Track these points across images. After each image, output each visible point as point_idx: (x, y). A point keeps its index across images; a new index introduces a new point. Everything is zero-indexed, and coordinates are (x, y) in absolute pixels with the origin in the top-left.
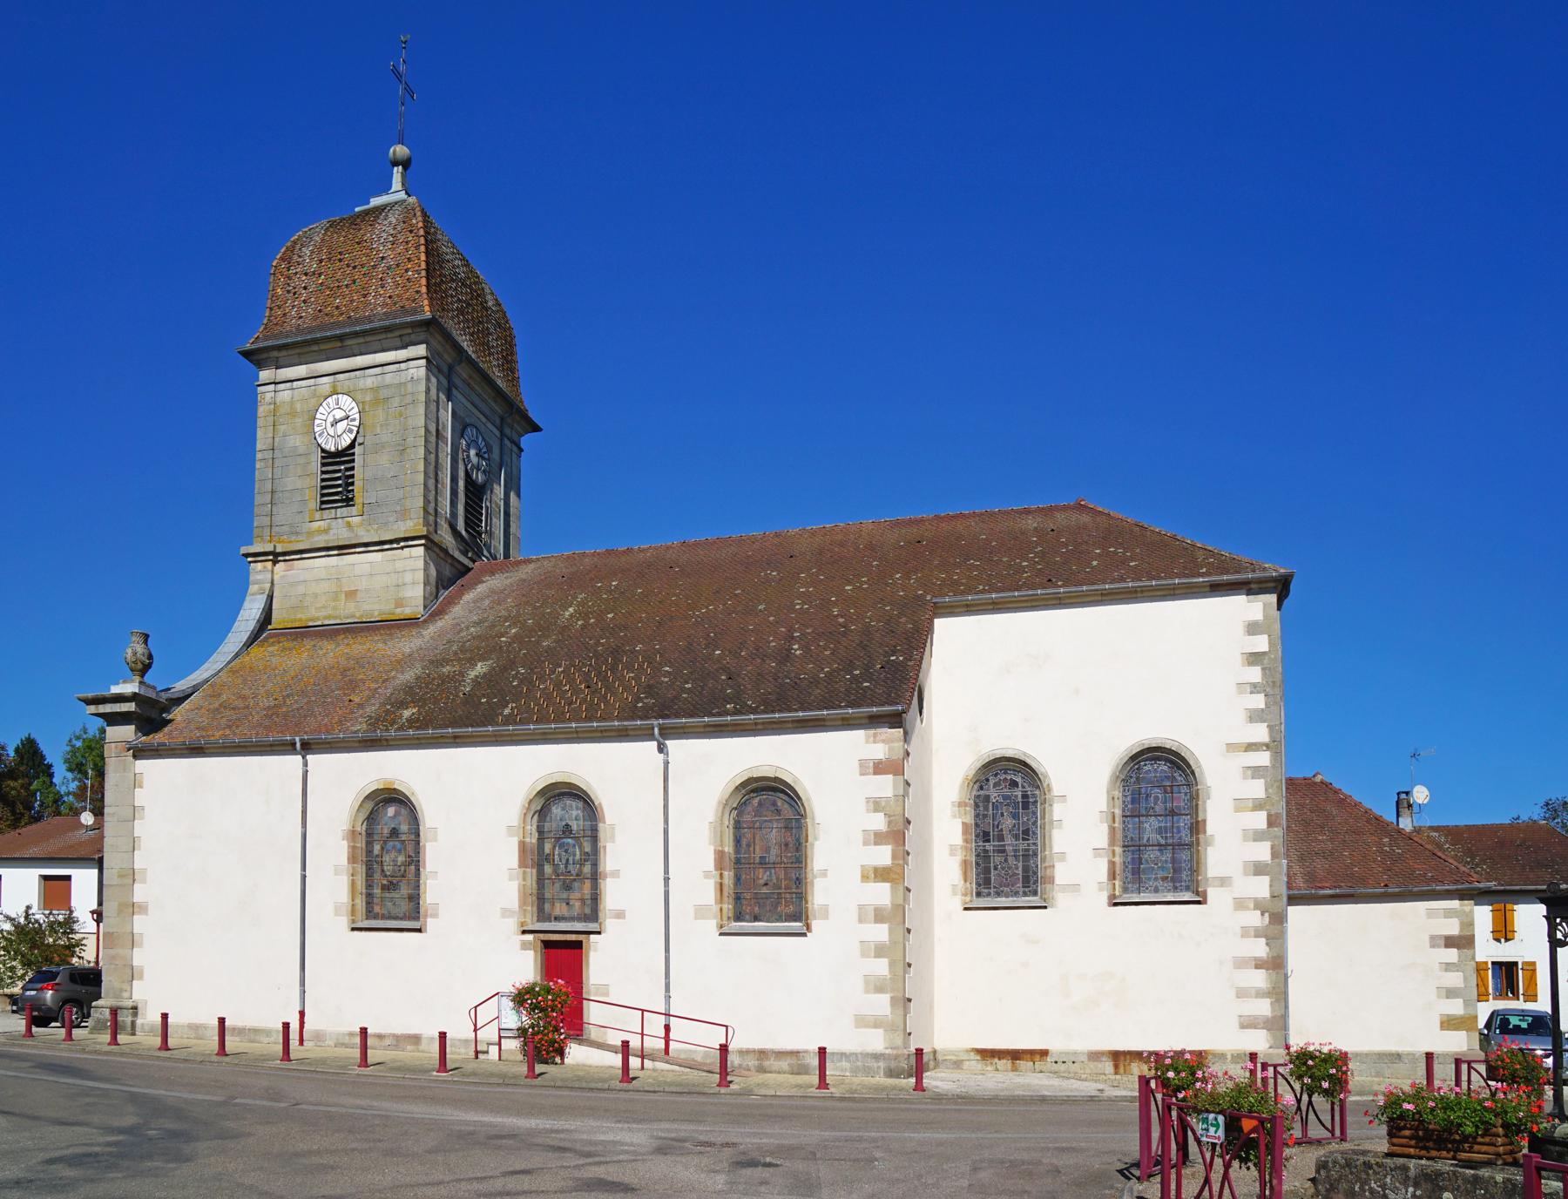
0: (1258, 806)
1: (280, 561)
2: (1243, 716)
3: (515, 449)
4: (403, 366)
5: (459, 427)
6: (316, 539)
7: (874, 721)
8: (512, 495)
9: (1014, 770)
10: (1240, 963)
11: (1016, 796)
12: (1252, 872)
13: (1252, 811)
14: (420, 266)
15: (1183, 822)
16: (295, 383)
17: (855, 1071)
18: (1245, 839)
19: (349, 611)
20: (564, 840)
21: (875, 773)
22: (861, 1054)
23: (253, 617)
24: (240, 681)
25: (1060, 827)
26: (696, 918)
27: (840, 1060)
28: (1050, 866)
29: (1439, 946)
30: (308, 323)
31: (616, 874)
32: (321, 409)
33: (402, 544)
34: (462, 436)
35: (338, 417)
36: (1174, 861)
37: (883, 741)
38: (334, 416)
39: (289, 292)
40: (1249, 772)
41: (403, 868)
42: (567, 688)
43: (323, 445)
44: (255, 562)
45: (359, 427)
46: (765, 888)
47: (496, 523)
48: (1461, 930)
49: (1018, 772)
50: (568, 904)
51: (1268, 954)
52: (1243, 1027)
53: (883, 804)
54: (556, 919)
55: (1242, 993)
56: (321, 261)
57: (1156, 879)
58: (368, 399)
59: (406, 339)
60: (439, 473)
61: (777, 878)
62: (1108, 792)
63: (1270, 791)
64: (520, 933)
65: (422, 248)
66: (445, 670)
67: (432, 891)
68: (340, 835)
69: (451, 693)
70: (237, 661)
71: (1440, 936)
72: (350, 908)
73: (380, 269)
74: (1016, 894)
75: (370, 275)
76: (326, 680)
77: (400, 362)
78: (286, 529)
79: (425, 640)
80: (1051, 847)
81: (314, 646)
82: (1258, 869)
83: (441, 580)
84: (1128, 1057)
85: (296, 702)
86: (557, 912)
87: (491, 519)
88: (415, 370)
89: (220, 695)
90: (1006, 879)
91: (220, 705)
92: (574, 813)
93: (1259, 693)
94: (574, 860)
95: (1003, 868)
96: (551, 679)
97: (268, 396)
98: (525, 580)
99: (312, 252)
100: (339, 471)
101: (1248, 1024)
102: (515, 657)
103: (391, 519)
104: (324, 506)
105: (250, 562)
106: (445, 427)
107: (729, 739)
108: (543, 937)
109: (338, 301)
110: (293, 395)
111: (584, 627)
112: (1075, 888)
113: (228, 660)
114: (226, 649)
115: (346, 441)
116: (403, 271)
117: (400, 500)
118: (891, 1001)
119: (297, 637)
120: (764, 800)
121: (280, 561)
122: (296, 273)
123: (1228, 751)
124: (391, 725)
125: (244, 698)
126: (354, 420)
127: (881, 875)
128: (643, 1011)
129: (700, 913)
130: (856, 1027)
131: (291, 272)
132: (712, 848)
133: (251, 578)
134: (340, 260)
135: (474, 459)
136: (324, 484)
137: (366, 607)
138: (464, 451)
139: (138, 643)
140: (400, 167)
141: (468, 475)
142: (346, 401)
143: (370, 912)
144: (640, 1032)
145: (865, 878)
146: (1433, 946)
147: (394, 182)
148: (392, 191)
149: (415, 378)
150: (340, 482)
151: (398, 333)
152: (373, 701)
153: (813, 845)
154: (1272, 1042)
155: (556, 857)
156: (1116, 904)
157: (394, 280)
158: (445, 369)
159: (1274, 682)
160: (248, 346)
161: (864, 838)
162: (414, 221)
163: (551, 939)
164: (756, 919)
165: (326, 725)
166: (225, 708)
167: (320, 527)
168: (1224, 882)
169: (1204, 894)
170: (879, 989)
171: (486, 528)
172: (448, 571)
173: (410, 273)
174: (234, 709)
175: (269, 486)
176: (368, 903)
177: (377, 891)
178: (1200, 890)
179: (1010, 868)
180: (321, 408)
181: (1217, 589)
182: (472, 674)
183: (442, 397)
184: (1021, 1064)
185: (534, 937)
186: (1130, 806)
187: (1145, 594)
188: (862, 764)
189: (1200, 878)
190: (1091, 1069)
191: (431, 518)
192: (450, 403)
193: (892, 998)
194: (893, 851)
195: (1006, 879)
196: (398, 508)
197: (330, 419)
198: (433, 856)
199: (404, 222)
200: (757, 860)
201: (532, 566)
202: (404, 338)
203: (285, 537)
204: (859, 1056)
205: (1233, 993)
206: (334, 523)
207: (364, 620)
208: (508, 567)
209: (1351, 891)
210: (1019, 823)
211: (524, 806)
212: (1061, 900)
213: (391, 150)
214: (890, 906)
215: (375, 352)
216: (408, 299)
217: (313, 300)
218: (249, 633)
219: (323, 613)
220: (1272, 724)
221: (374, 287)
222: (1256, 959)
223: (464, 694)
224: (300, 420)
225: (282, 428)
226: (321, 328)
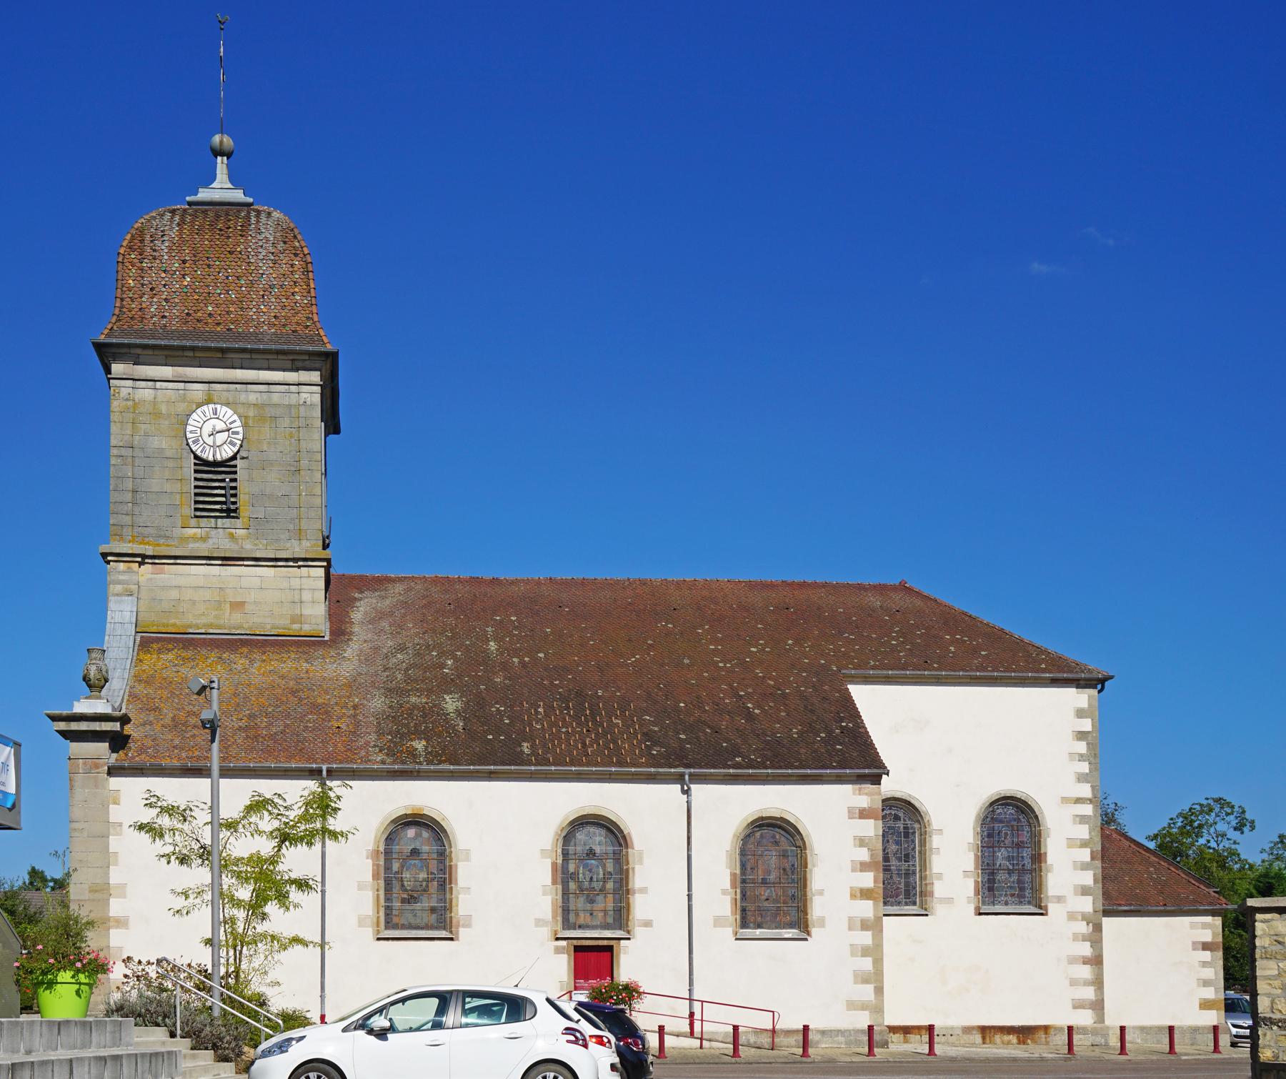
0: (1084, 844)
2: (1073, 778)
4: (293, 388)
7: (860, 779)
9: (897, 807)
10: (1072, 960)
11: (899, 827)
12: (1080, 893)
13: (1080, 847)
15: (1026, 853)
17: (848, 1043)
18: (1075, 868)
19: (233, 622)
20: (588, 861)
21: (860, 818)
22: (853, 1030)
25: (938, 853)
26: (715, 926)
27: (837, 1036)
28: (930, 884)
29: (1198, 950)
31: (644, 890)
33: (300, 563)
35: (218, 428)
36: (1019, 881)
37: (866, 794)
40: (1078, 819)
41: (424, 884)
43: (198, 453)
45: (242, 441)
46: (766, 902)
48: (1213, 938)
49: (901, 809)
50: (591, 914)
51: (1092, 953)
52: (1075, 1007)
53: (867, 841)
54: (580, 927)
55: (1074, 983)
56: (184, 262)
57: (1006, 895)
58: (251, 414)
59: (300, 364)
61: (777, 895)
62: (974, 829)
63: (1093, 833)
64: (553, 940)
67: (464, 904)
68: (365, 854)
71: (1199, 942)
72: (375, 920)
74: (899, 903)
80: (931, 869)
82: (1085, 891)
84: (992, 1031)
86: (581, 921)
88: (308, 395)
90: (892, 892)
92: (598, 839)
93: (1084, 761)
94: (597, 878)
95: (889, 883)
97: (124, 392)
99: (170, 248)
100: (223, 480)
101: (1078, 1005)
103: (282, 537)
107: (724, 786)
108: (575, 942)
110: (156, 395)
112: (949, 901)
115: (227, 452)
118: (875, 990)
120: (765, 833)
123: (1062, 803)
126: (237, 433)
127: (866, 895)
128: (702, 1002)
129: (718, 922)
130: (847, 1010)
132: (729, 871)
142: (225, 412)
143: (388, 923)
144: (700, 1019)
145: (853, 896)
146: (1194, 949)
147: (218, 171)
148: (210, 187)
149: (308, 403)
153: (811, 870)
154: (1096, 1019)
155: (581, 875)
156: (980, 914)
159: (1095, 754)
160: (102, 338)
161: (852, 866)
163: (584, 944)
164: (759, 926)
167: (195, 534)
168: (1060, 899)
169: (1046, 908)
170: (866, 981)
176: (387, 915)
177: (397, 904)
178: (1043, 905)
179: (894, 883)
181: (1055, 682)
184: (911, 1037)
185: (568, 942)
186: (986, 839)
187: (1003, 681)
188: (851, 812)
189: (1042, 896)
190: (965, 1040)
193: (875, 987)
194: (874, 876)
195: (892, 892)
198: (464, 874)
199: (285, 243)
200: (760, 881)
202: (296, 362)
204: (852, 1032)
205: (1067, 982)
206: (214, 532)
207: (258, 633)
209: (1139, 908)
210: (901, 849)
211: (557, 833)
212: (939, 909)
214: (873, 918)
215: (259, 369)
219: (204, 620)
220: (1095, 784)
222: (1083, 957)
224: (167, 422)
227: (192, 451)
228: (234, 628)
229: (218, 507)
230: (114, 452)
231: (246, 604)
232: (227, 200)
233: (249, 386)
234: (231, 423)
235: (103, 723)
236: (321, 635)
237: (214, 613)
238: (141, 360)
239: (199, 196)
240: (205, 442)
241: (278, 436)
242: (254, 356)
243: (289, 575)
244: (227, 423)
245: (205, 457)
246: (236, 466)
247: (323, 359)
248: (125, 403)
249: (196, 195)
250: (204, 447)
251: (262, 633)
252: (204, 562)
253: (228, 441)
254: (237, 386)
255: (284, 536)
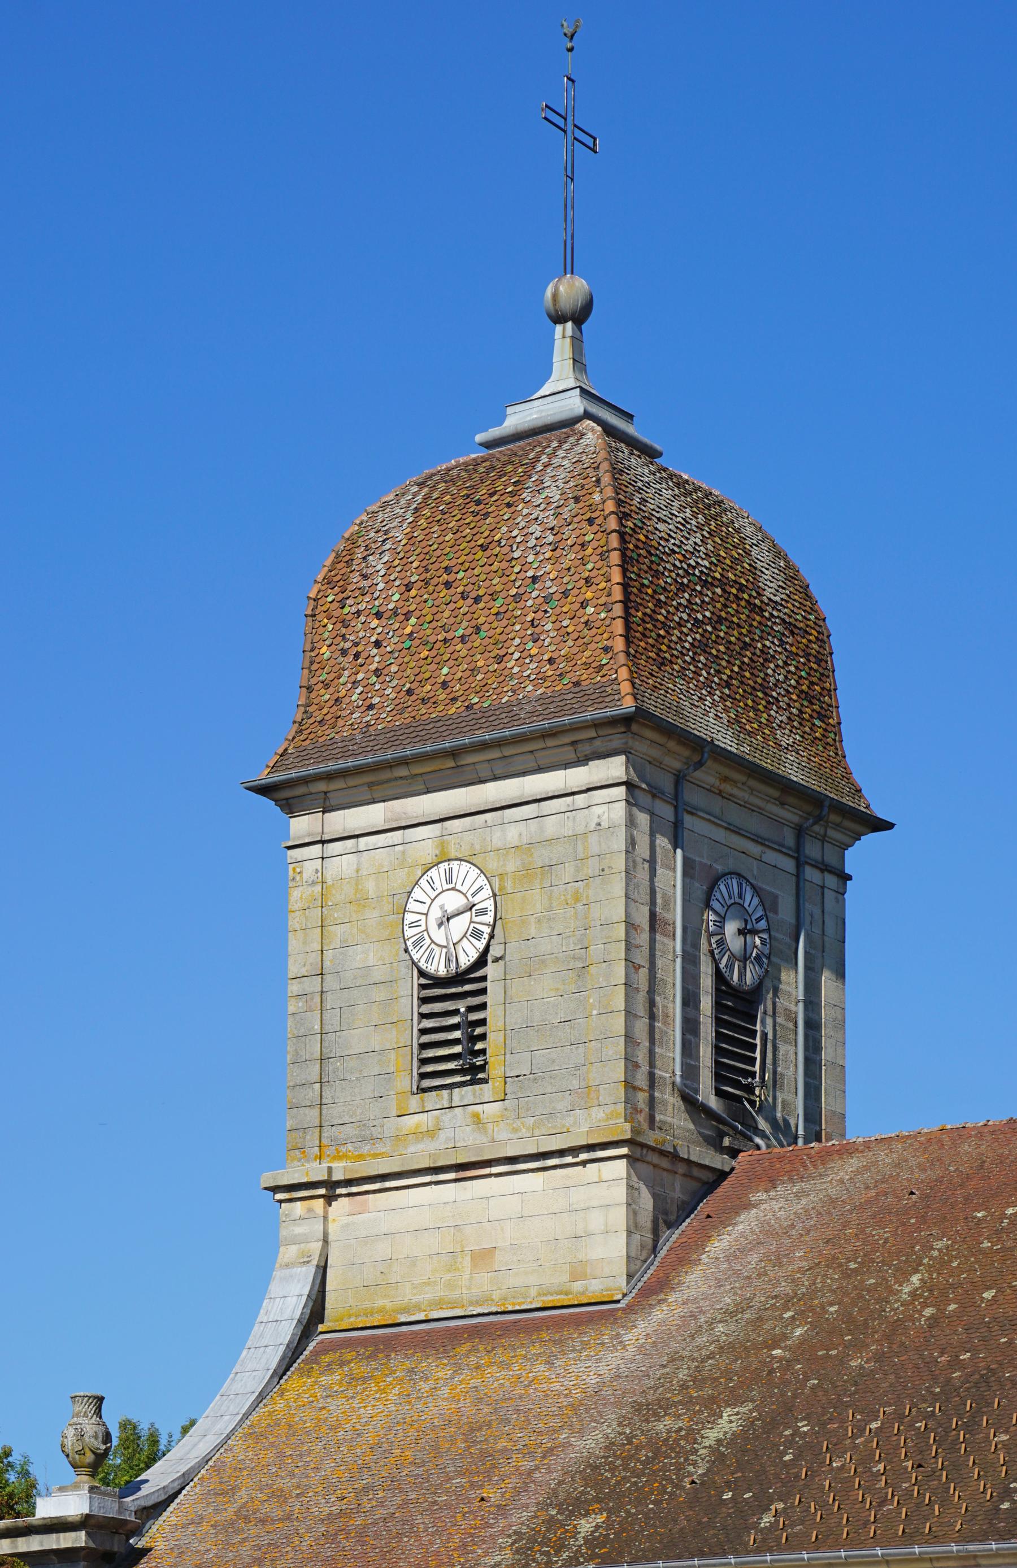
1: (341, 1195)
3: (831, 881)
4: (580, 800)
5: (700, 889)
6: (412, 1149)
8: (826, 979)
14: (609, 595)
16: (362, 840)
23: (287, 1315)
24: (270, 1456)
30: (384, 719)
32: (417, 893)
33: (583, 1156)
34: (708, 905)
35: (450, 909)
38: (442, 907)
39: (344, 652)
42: (881, 1467)
43: (422, 965)
44: (290, 1200)
45: (494, 927)
47: (787, 1052)
56: (408, 587)
58: (510, 867)
59: (586, 749)
60: (657, 999)
65: (615, 557)
66: (660, 1427)
69: (670, 1481)
70: (261, 1410)
73: (530, 603)
75: (509, 614)
76: (436, 1451)
77: (573, 794)
78: (349, 1131)
79: (628, 1355)
81: (411, 1371)
83: (666, 1213)
85: (381, 1504)
87: (775, 1049)
89: (234, 1489)
91: (237, 1513)
96: (855, 1447)
97: (310, 869)
98: (833, 1201)
99: (389, 567)
100: (456, 1012)
102: (795, 1396)
104: (427, 1083)
105: (281, 1201)
106: (667, 904)
109: (445, 670)
110: (359, 864)
111: (934, 1322)
113: (243, 1411)
114: (237, 1387)
115: (468, 954)
116: (577, 606)
117: (577, 1067)
119: (377, 1350)
121: (341, 1195)
122: (358, 613)
124: (558, 1553)
125: (280, 1496)
126: (483, 912)
131: (346, 610)
133: (283, 1233)
134: (448, 585)
135: (735, 943)
136: (426, 1039)
137: (514, 1281)
138: (711, 935)
139: (85, 1415)
140: (569, 325)
141: (719, 977)
142: (467, 875)
147: (556, 358)
149: (605, 824)
150: (457, 1034)
151: (567, 739)
152: (524, 1500)
157: (558, 625)
158: (667, 784)
162: (597, 497)
165: (437, 1553)
166: (247, 1520)
167: (418, 1125)
171: (762, 1077)
172: (677, 1190)
173: (590, 610)
174: (263, 1521)
175: (315, 1049)
180: (417, 890)
182: (712, 1435)
183: (663, 842)
191: (642, 1097)
192: (679, 851)
196: (575, 1084)
197: (436, 914)
199: (577, 500)
201: (854, 1163)
203: (350, 1147)
206: (447, 1116)
207: (510, 1308)
208: (805, 1166)
213: (549, 292)
215: (524, 774)
216: (587, 665)
217: (394, 668)
218: (283, 1348)
221: (517, 641)
223: (693, 1482)
224: (375, 914)
225: (337, 932)
226: (414, 730)
227: (413, 963)
228: (471, 1304)
229: (451, 1065)
230: (294, 988)
231: (497, 1251)
232: (540, 423)
233: (507, 812)
234: (474, 895)
235: (62, 1535)
236: (615, 1298)
237: (446, 1277)
238: (333, 802)
239: (507, 423)
240: (433, 942)
241: (554, 904)
242: (508, 751)
243: (568, 1183)
244: (469, 895)
245: (432, 971)
246: (484, 978)
247: (623, 729)
248: (310, 889)
249: (501, 423)
250: (432, 950)
251: (518, 1308)
252: (427, 1179)
253: (469, 933)
254: (488, 816)
255: (562, 1104)
